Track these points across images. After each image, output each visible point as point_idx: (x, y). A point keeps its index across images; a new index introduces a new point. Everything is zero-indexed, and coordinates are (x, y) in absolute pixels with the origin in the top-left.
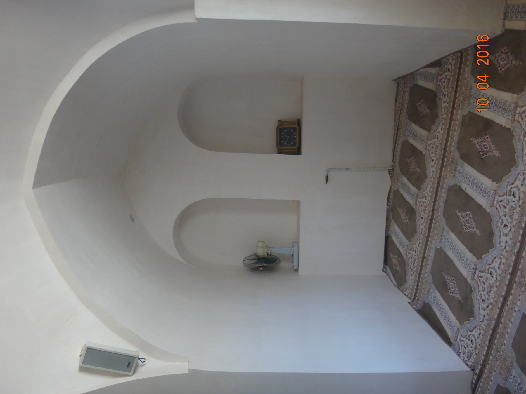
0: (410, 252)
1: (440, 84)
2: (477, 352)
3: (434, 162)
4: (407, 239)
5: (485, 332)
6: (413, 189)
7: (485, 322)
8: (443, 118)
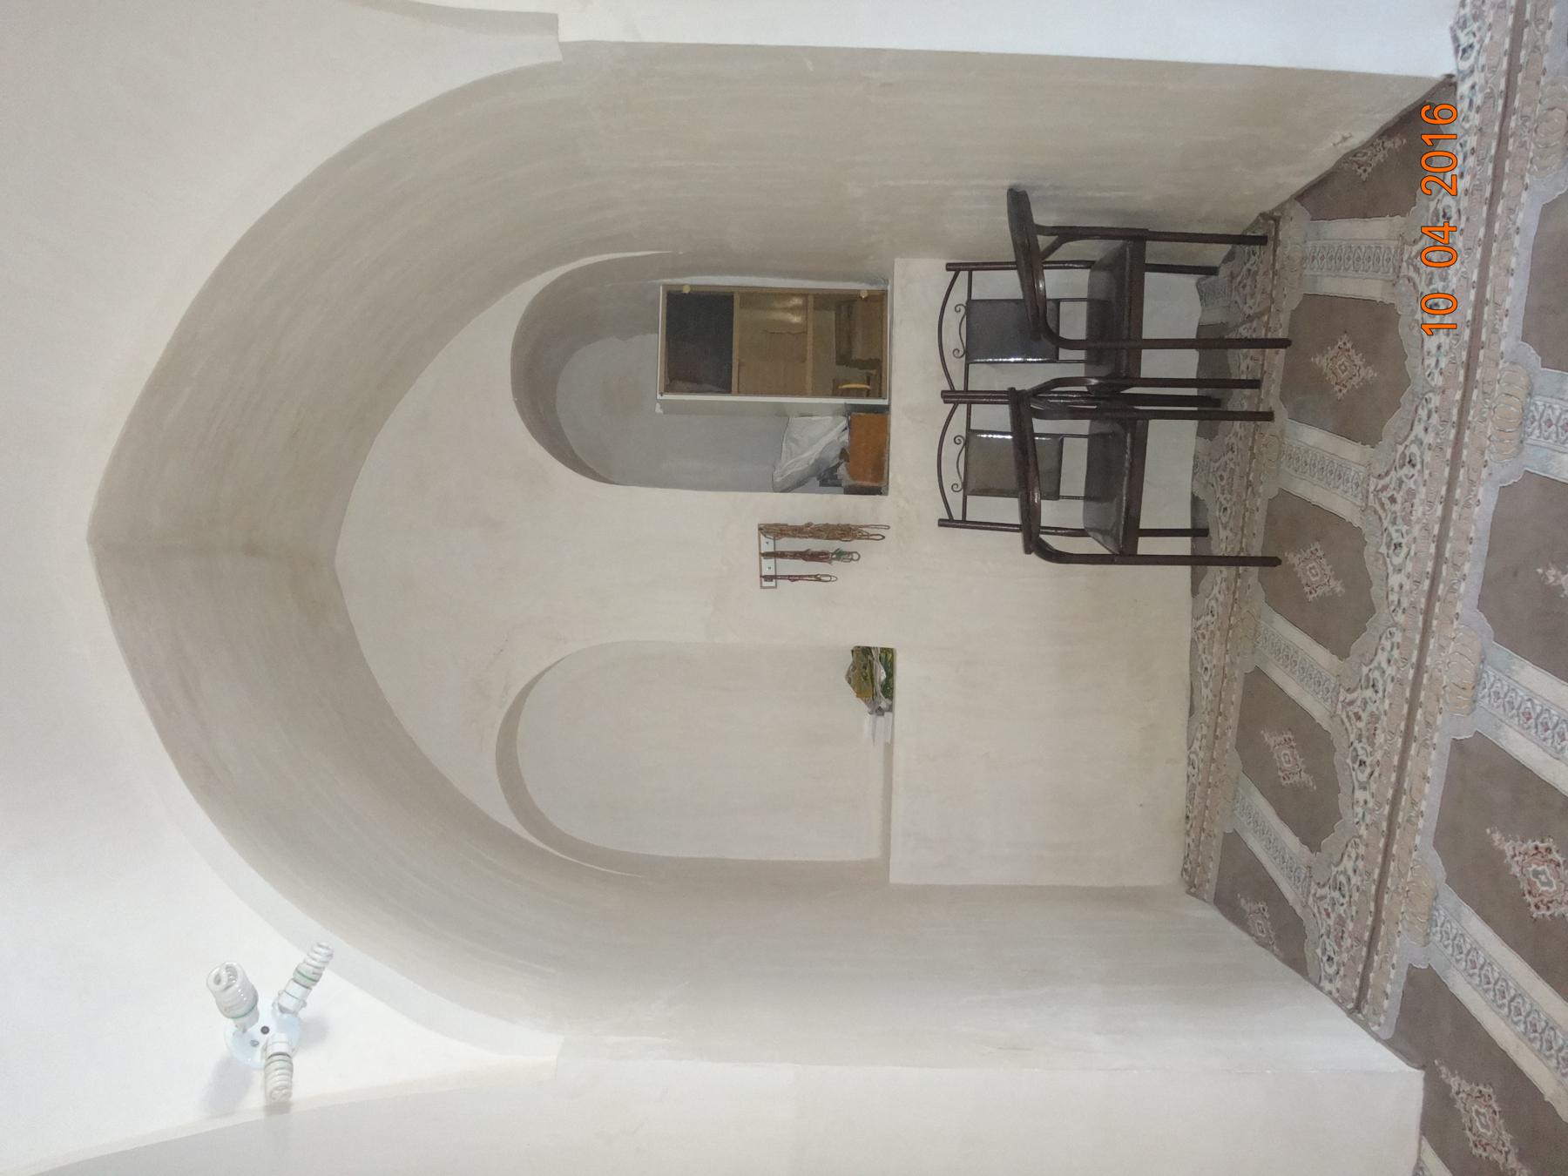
0: (1321, 892)
1: (1412, 274)
3: (1405, 550)
4: (1304, 842)
6: (1321, 656)
8: (1395, 625)
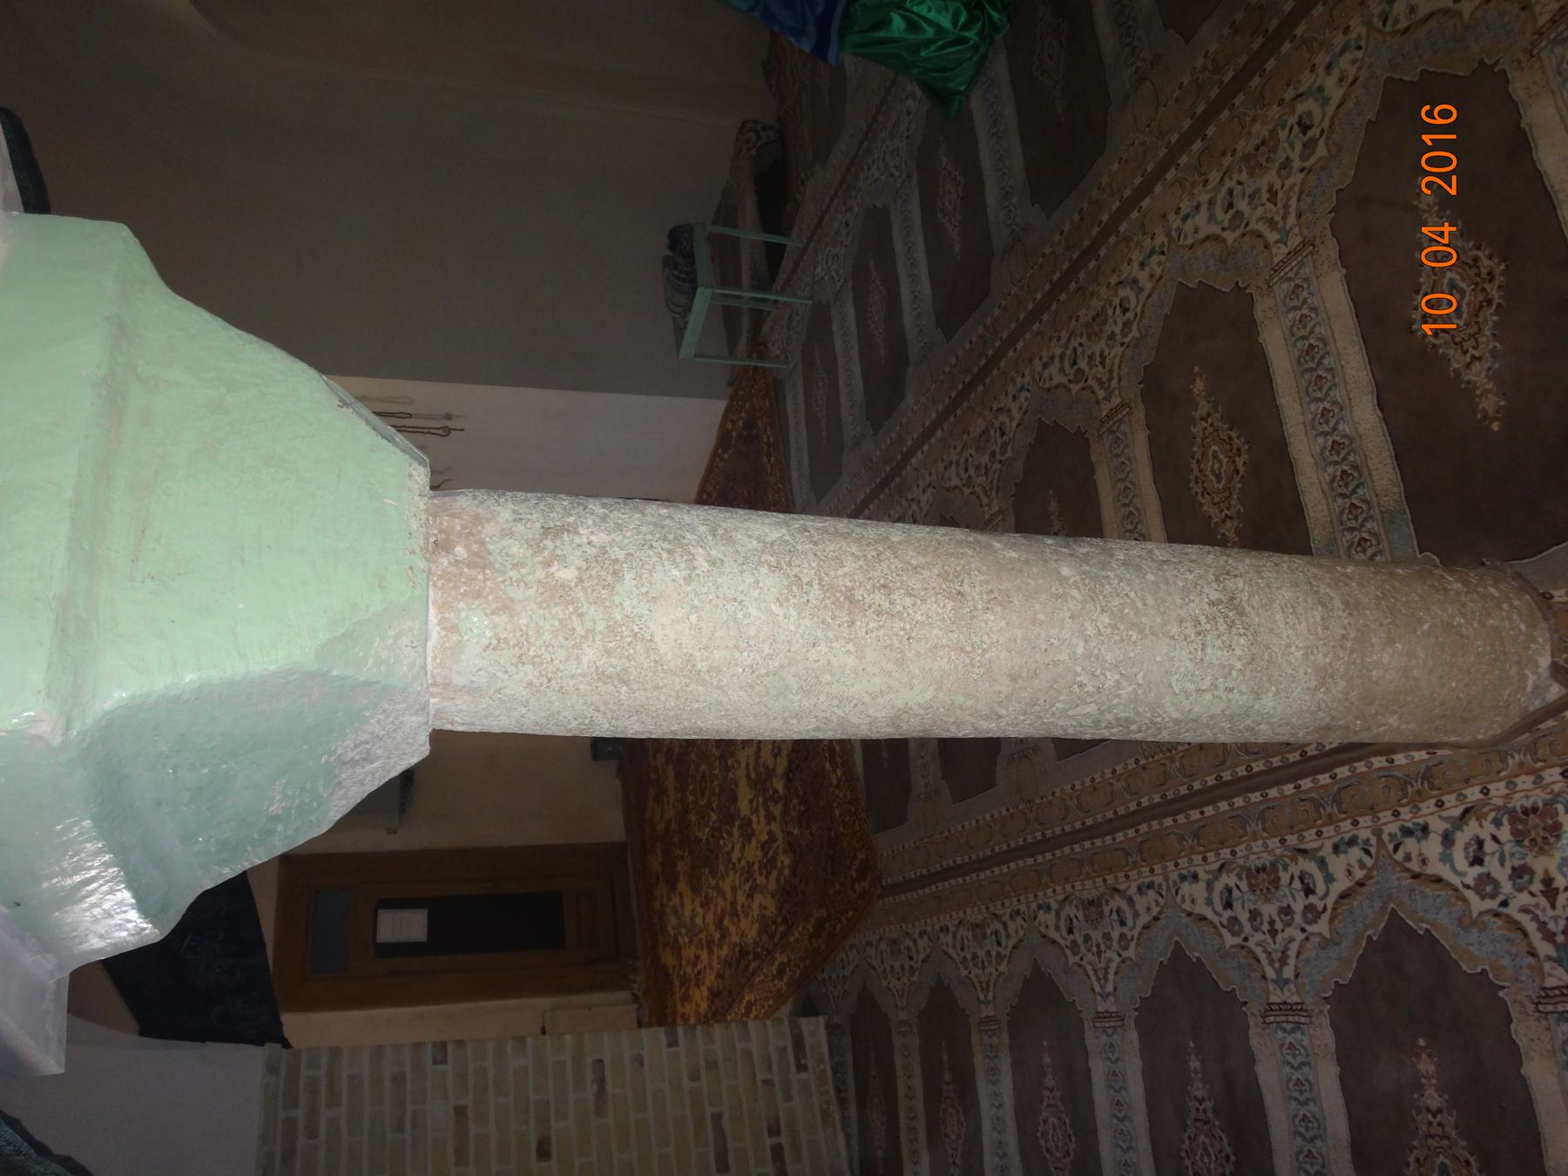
2: (1073, 323)
5: (1164, 216)
7: (1147, 243)
